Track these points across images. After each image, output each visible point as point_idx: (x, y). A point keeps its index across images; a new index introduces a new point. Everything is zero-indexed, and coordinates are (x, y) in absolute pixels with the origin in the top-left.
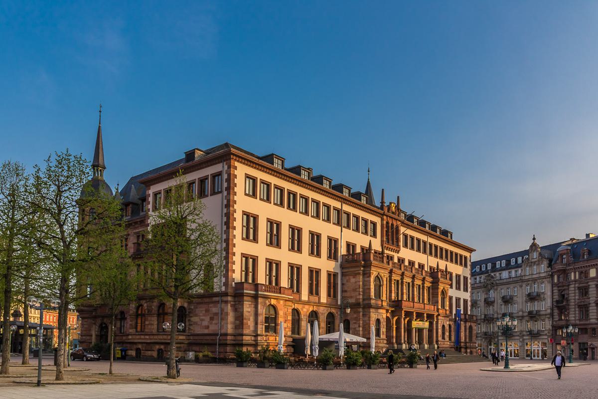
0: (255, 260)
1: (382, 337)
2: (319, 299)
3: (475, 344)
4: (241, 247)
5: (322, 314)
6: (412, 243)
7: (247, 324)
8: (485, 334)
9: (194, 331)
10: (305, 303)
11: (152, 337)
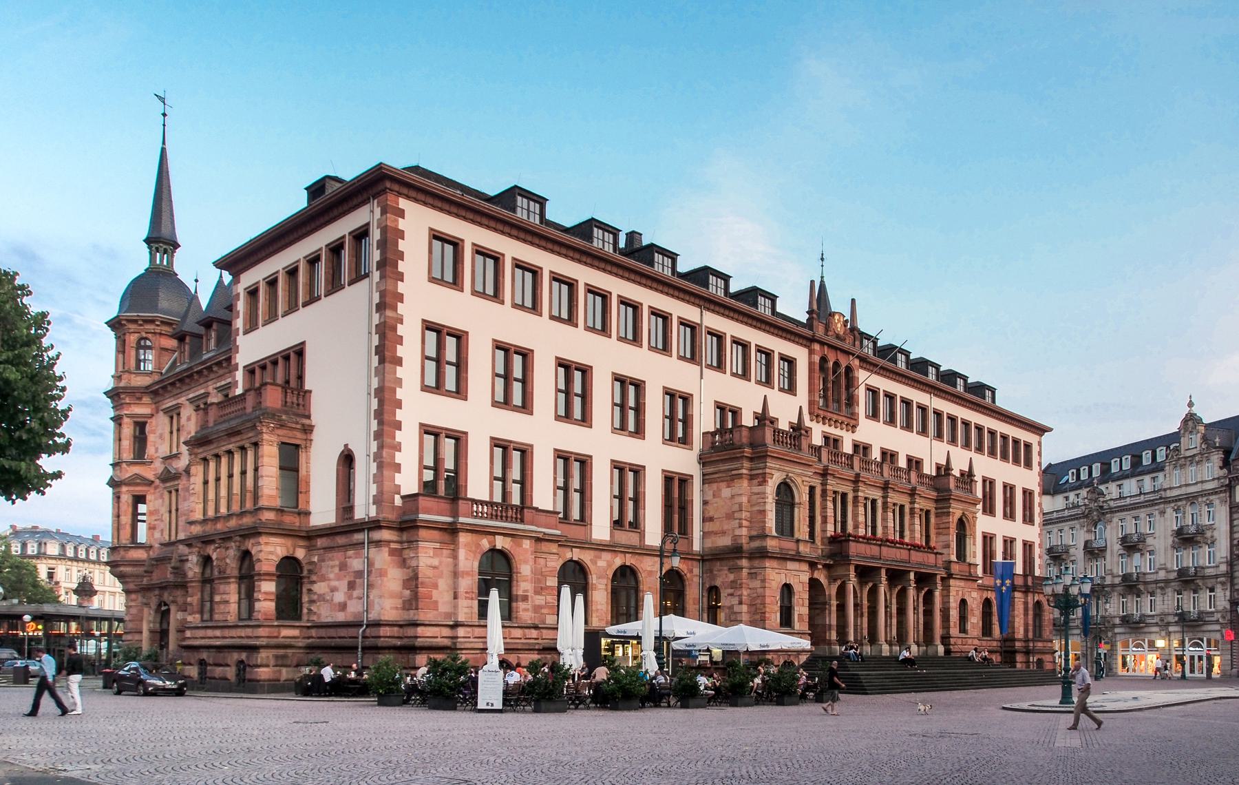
0: (585, 462)
2: (642, 535)
4: (417, 407)
5: (650, 573)
6: (888, 410)
9: (319, 616)
11: (227, 633)
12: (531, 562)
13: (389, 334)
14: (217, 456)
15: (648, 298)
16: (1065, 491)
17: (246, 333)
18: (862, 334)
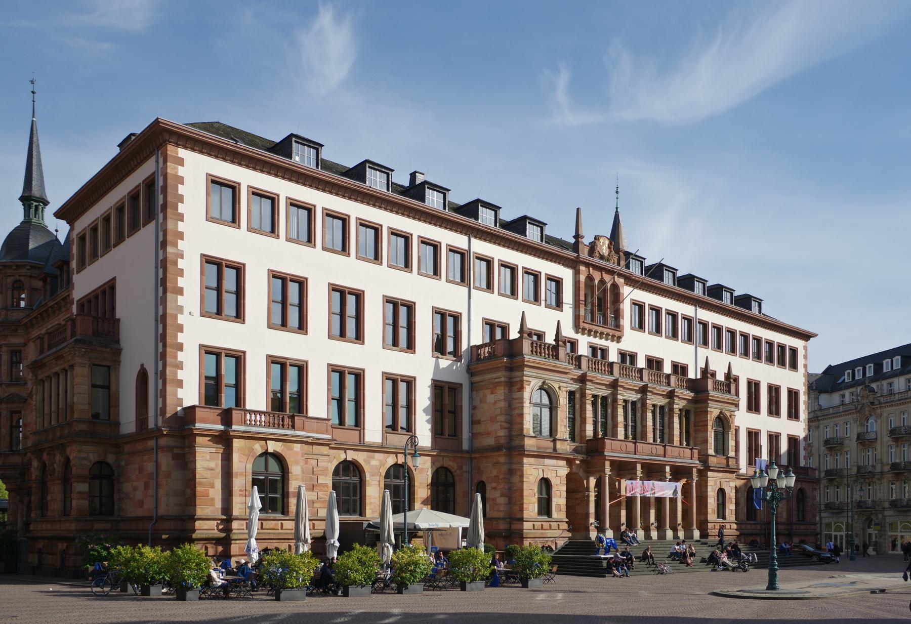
1: (555, 514)
3: (812, 527)
6: (650, 321)
7: (207, 495)
8: (860, 505)
10: (373, 449)
12: (302, 463)
13: (170, 268)
14: (50, 378)
15: (417, 228)
16: (841, 389)
17: (78, 273)
18: (628, 254)
